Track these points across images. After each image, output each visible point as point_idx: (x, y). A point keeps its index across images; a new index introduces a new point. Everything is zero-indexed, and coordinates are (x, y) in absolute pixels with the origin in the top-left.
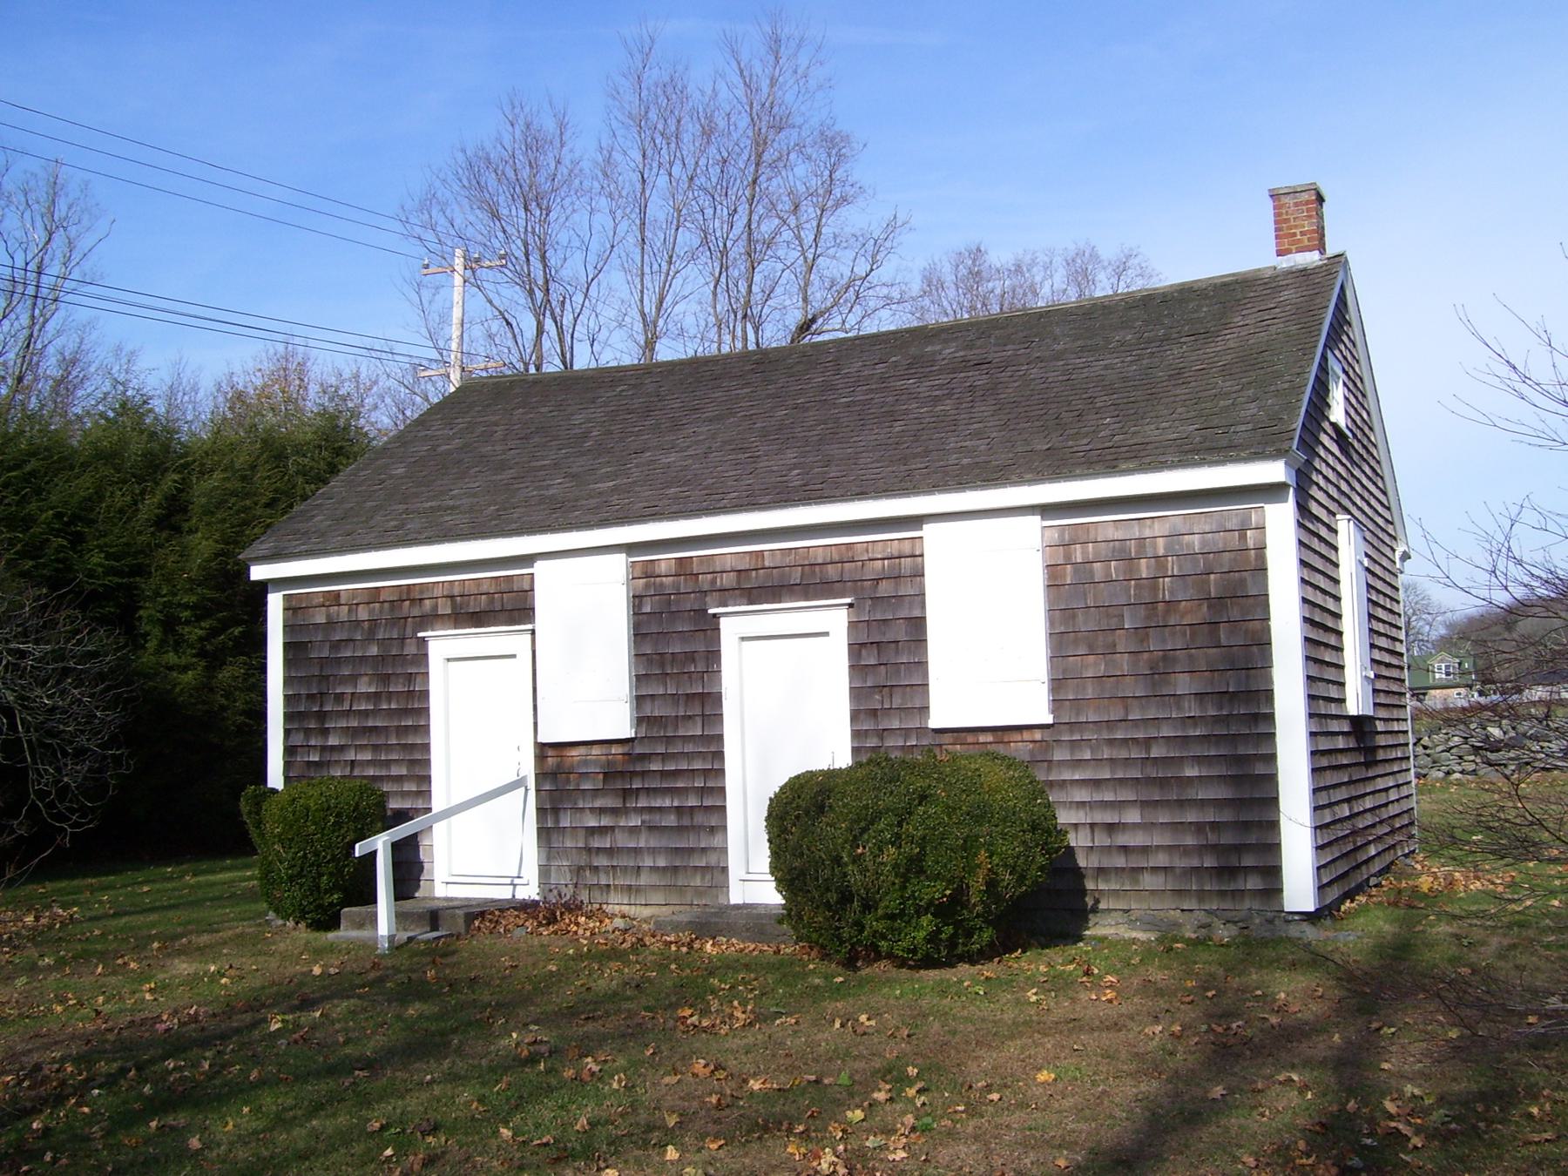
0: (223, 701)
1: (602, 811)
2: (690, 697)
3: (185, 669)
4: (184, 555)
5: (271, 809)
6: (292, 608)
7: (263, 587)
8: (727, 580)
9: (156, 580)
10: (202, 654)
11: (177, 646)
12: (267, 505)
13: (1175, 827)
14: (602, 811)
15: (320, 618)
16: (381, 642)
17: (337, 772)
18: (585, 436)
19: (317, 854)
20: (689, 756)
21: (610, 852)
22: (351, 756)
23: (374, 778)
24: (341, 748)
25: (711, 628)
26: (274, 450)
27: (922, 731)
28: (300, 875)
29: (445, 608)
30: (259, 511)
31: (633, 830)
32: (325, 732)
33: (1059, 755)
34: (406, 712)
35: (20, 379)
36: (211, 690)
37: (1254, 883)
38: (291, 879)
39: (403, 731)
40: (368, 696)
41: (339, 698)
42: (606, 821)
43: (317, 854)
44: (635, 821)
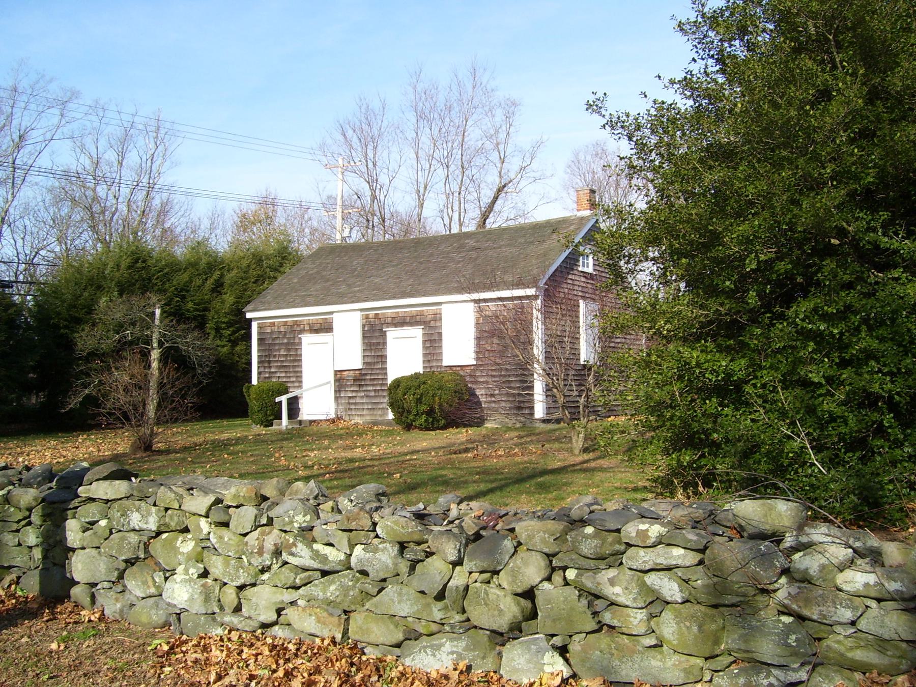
0: (238, 359)
1: (353, 391)
2: (378, 356)
3: (223, 346)
4: (223, 302)
5: (252, 390)
6: (260, 327)
7: (250, 320)
8: (389, 320)
9: (212, 313)
10: (230, 341)
11: (221, 337)
12: (254, 283)
13: (508, 394)
14: (353, 391)
15: (269, 331)
16: (288, 338)
17: (274, 380)
18: (355, 270)
19: (266, 404)
20: (378, 374)
21: (355, 404)
22: (278, 375)
23: (285, 382)
24: (275, 372)
25: (384, 335)
26: (258, 259)
27: (441, 367)
28: (261, 410)
29: (307, 328)
30: (251, 285)
31: (362, 397)
32: (270, 367)
33: (478, 374)
34: (295, 361)
35: (144, 212)
36: (233, 355)
37: (527, 411)
38: (258, 411)
39: (294, 367)
40: (283, 356)
41: (275, 356)
42: (354, 394)
43: (266, 404)
44: (362, 394)
